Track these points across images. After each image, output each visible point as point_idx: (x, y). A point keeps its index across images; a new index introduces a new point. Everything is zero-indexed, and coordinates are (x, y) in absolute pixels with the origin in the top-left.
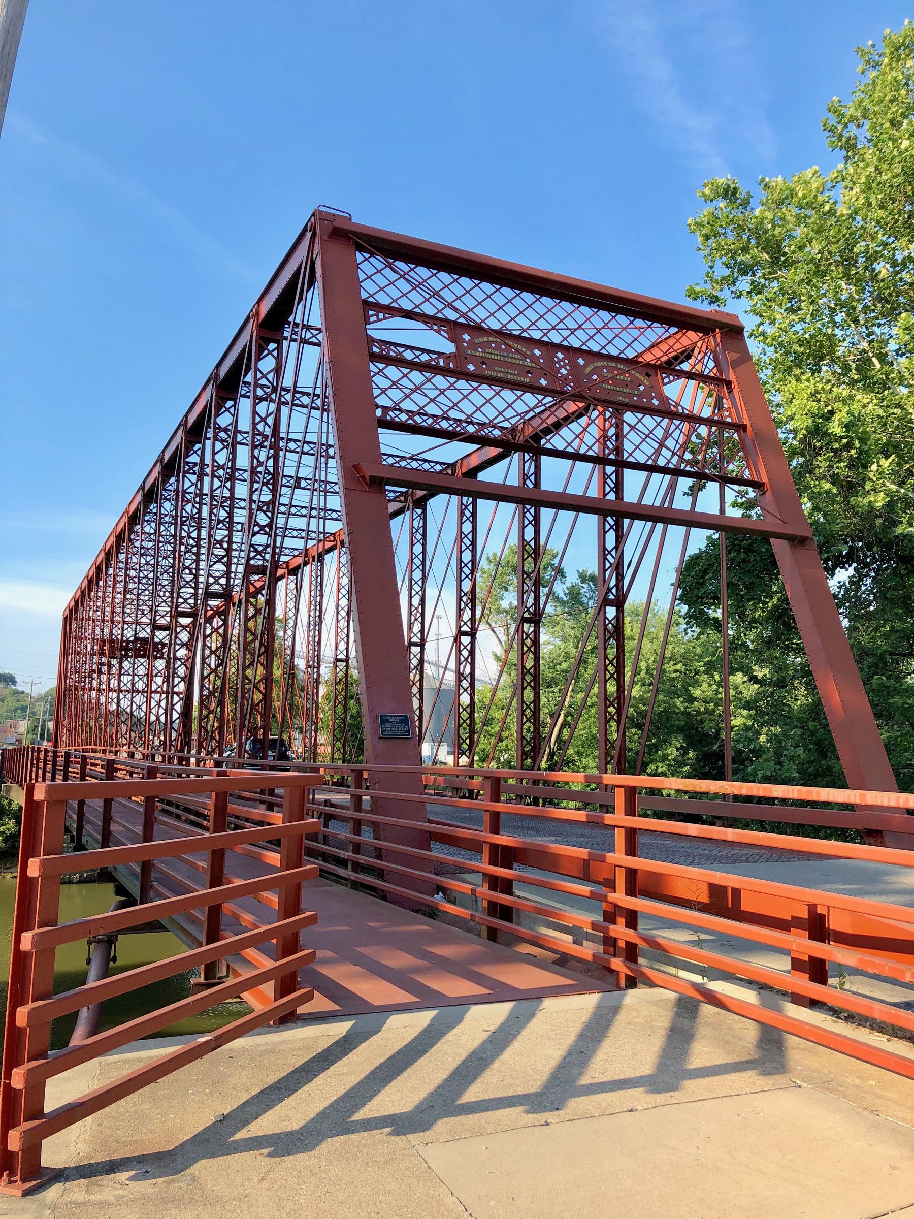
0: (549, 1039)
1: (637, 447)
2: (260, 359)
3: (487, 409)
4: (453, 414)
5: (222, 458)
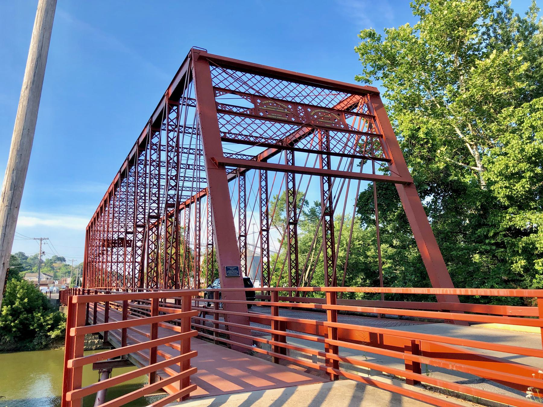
0: (300, 402)
1: (335, 146)
2: (170, 113)
3: (269, 132)
4: (254, 134)
5: (154, 157)
